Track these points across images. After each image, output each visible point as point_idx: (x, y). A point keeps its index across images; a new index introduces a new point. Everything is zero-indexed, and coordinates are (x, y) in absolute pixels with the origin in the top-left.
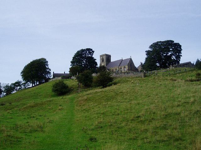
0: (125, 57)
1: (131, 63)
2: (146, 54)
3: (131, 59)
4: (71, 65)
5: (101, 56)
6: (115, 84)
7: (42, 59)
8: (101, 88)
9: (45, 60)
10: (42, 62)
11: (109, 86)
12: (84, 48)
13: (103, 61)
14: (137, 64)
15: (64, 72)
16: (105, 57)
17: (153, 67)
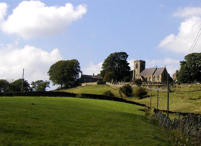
0: (161, 66)
1: (165, 74)
2: (181, 65)
3: (165, 68)
4: (102, 68)
5: (135, 62)
6: (149, 96)
7: (74, 60)
8: (139, 99)
9: (77, 62)
10: (74, 63)
11: (144, 98)
12: (118, 51)
13: (137, 67)
14: (172, 72)
15: (94, 74)
16: (139, 63)
17: (186, 79)
